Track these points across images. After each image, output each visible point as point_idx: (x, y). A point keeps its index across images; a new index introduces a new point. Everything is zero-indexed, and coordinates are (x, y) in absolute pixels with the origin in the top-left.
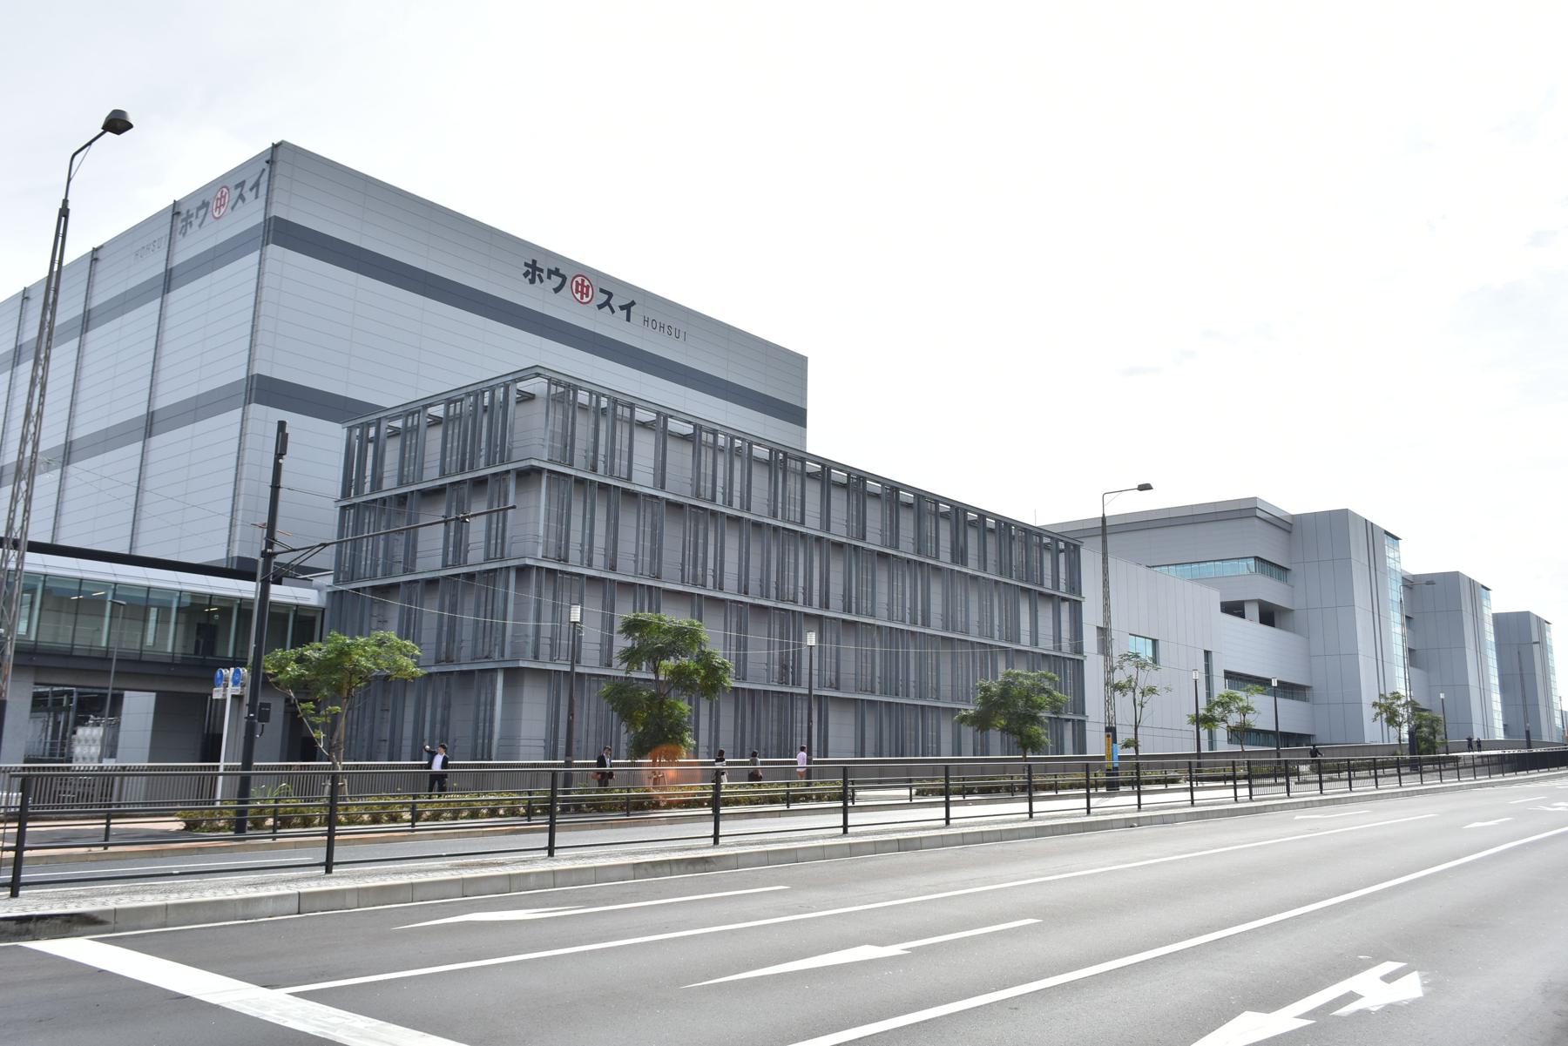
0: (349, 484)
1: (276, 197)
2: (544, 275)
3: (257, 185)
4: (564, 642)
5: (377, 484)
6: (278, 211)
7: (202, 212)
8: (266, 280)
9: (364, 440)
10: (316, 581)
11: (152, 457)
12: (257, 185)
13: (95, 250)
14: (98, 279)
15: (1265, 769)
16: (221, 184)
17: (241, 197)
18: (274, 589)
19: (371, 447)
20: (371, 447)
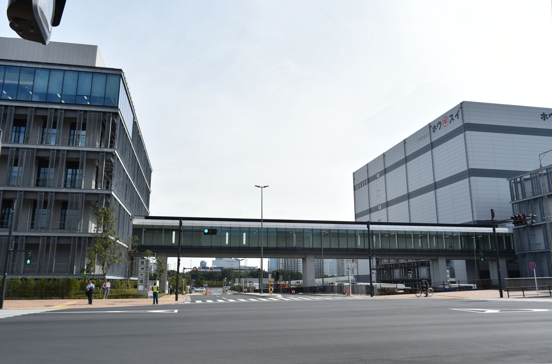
1: (465, 117)
2: (548, 117)
3: (457, 115)
5: (524, 195)
7: (439, 125)
9: (516, 183)
10: (507, 225)
12: (457, 115)
13: (404, 140)
15: (9, 174)
16: (444, 116)
18: (496, 229)
19: (519, 185)
20: (519, 185)
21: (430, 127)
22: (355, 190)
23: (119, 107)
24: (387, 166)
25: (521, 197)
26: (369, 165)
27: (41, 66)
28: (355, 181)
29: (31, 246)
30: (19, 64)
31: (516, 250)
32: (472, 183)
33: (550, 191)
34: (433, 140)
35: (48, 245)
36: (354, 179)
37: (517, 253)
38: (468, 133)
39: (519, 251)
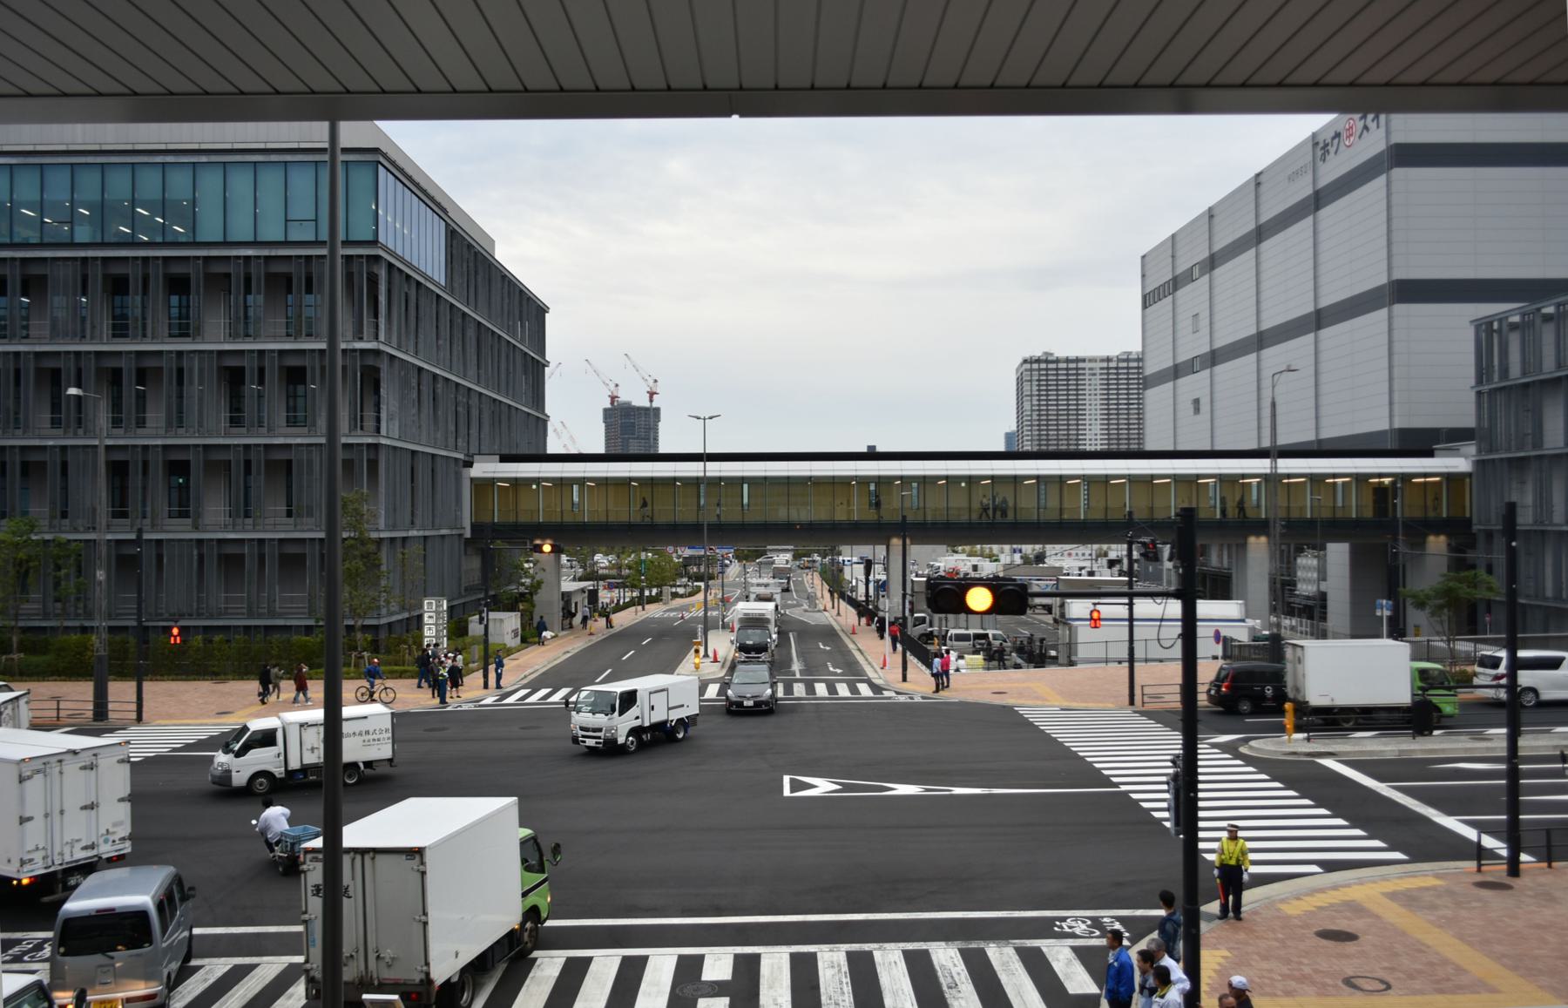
0: (1482, 373)
4: (101, 575)
5: (1505, 372)
6: (399, 708)
8: (1395, 199)
11: (1217, 379)
13: (1258, 175)
14: (1263, 199)
17: (1366, 128)
20: (1514, 341)
21: (1316, 144)
22: (1145, 306)
23: (381, 239)
24: (1217, 247)
25: (1496, 377)
26: (1178, 238)
27: (204, 159)
28: (1148, 281)
29: (230, 559)
30: (159, 159)
31: (1475, 520)
32: (1397, 323)
33: (1559, 366)
34: (1322, 183)
35: (262, 558)
36: (1143, 276)
37: (1475, 528)
38: (1398, 173)
39: (1480, 523)
